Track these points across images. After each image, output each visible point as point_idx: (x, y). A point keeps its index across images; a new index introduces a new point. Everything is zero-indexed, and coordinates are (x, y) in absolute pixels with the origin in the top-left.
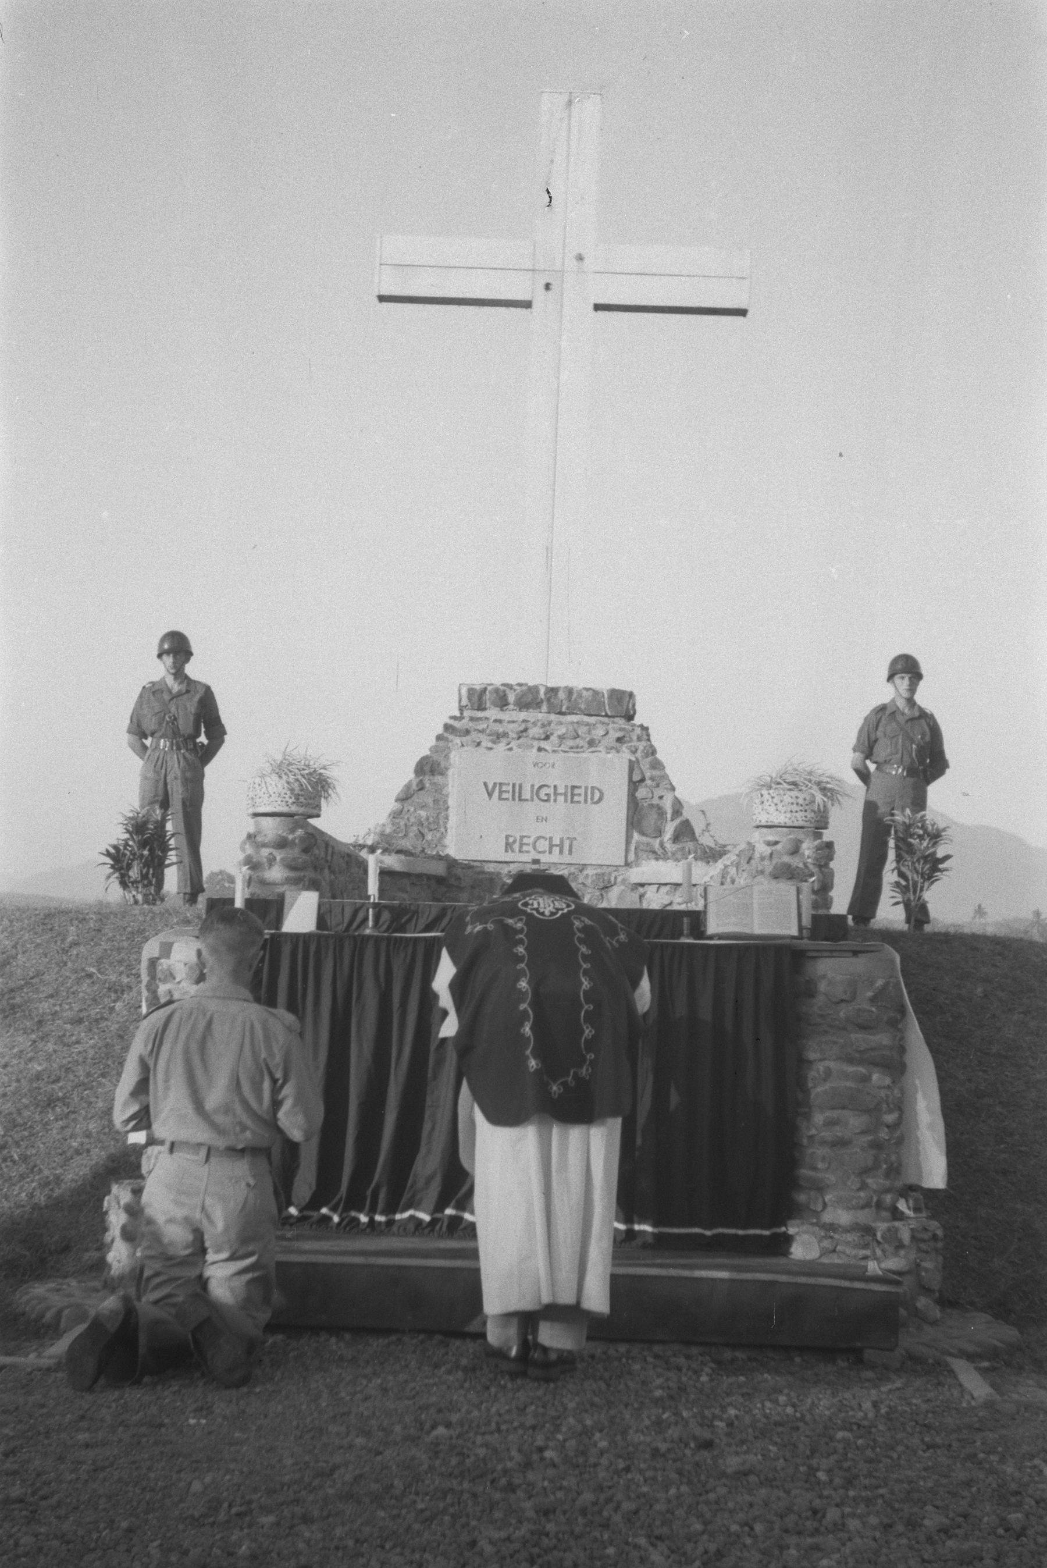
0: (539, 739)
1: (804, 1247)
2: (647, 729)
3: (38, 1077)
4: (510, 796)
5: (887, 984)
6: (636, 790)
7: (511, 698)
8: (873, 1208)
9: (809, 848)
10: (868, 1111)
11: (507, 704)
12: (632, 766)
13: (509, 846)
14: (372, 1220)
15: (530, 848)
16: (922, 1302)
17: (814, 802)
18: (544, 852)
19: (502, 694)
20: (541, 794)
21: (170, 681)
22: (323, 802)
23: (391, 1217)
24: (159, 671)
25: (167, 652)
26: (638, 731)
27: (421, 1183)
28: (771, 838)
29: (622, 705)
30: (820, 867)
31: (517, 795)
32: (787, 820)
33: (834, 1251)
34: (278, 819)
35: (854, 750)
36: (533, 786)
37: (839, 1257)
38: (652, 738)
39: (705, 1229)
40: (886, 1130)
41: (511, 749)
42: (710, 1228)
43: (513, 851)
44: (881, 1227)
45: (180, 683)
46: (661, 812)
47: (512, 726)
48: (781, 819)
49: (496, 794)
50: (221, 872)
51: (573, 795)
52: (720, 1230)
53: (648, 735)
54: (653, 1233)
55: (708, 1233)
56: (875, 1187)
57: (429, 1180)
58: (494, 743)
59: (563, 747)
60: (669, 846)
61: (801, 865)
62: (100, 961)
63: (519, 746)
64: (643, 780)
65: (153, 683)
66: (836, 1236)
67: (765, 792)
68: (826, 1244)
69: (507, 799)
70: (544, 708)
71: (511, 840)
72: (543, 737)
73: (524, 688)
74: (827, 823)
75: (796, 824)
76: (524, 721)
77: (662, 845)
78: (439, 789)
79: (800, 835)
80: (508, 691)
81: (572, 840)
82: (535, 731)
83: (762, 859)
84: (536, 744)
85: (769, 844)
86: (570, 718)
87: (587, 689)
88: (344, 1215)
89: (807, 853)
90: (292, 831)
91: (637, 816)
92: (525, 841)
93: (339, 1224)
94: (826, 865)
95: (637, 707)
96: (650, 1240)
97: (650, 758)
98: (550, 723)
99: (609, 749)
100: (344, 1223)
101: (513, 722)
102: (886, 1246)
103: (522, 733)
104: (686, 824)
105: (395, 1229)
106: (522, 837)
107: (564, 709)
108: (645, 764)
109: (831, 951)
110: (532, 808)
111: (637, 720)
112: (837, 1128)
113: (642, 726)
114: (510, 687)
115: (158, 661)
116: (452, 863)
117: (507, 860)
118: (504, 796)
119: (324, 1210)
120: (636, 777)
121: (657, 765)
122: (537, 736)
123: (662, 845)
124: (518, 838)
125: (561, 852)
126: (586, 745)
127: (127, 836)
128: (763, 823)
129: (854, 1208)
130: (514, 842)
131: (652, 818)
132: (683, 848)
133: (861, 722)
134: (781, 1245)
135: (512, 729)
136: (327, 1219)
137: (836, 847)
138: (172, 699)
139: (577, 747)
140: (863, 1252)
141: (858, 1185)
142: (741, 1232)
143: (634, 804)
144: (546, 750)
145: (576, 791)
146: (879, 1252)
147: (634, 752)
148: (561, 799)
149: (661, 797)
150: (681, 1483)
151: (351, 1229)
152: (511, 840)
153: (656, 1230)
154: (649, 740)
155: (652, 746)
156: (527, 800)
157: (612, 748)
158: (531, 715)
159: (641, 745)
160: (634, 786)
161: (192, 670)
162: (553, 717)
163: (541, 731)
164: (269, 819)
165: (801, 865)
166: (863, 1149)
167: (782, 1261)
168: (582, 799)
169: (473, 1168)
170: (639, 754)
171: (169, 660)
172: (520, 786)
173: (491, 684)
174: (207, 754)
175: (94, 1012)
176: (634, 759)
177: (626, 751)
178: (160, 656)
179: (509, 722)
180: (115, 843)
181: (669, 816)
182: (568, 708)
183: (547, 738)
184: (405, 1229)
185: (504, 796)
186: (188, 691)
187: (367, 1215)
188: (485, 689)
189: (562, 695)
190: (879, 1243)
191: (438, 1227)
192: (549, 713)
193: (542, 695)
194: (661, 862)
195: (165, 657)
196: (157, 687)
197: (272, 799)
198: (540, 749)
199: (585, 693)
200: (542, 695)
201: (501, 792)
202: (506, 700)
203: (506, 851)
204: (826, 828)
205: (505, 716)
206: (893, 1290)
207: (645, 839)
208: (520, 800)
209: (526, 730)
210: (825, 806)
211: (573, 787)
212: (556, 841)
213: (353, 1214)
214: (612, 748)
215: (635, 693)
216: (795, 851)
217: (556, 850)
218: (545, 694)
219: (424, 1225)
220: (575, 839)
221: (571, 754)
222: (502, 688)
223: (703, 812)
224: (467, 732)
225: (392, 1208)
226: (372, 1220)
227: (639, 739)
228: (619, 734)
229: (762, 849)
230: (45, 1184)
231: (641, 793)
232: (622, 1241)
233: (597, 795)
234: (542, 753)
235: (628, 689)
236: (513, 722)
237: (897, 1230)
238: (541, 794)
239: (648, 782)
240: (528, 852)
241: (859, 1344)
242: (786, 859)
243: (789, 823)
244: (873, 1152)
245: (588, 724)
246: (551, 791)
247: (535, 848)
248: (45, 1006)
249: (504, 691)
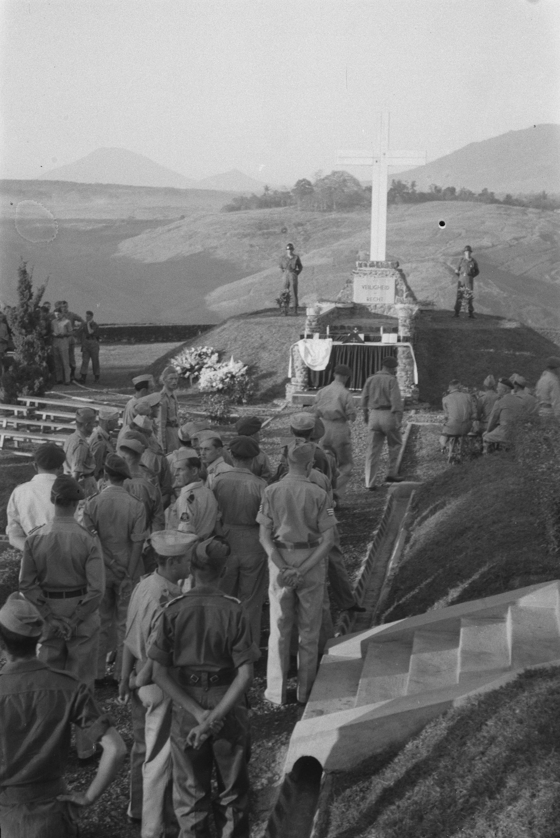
3: (271, 362)
12: (396, 281)
13: (368, 300)
16: (414, 401)
44: (407, 390)
50: (304, 180)
60: (405, 299)
62: (279, 337)
78: (352, 287)
82: (374, 273)
103: (371, 273)
116: (355, 304)
131: (400, 293)
150: (525, 479)
160: (396, 285)
174: (298, 273)
175: (280, 349)
224: (358, 273)
230: (274, 382)
231: (398, 287)
248: (270, 347)
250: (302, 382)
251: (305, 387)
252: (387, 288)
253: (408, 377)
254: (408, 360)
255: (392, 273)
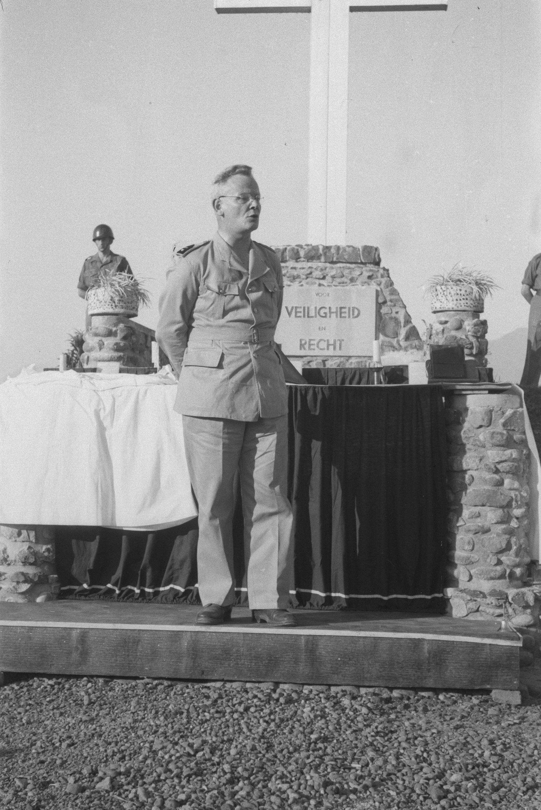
0: (319, 279)
1: (459, 607)
2: (388, 270)
4: (302, 314)
5: (515, 413)
6: (381, 308)
7: (302, 253)
8: (508, 580)
9: (469, 325)
10: (502, 507)
11: (299, 258)
13: (302, 346)
14: (143, 592)
15: (315, 347)
17: (472, 293)
18: (324, 349)
19: (296, 251)
20: (322, 313)
21: (101, 255)
22: (141, 305)
23: (157, 589)
24: (94, 249)
25: (99, 239)
26: (381, 271)
27: (176, 566)
28: (443, 319)
29: (371, 257)
30: (477, 338)
31: (306, 314)
32: (454, 306)
33: (477, 611)
34: (106, 317)
35: (523, 283)
36: (316, 308)
37: (482, 615)
38: (390, 276)
39: (383, 595)
40: (515, 520)
41: (302, 285)
42: (387, 595)
43: (305, 349)
45: (107, 257)
46: (396, 320)
47: (302, 271)
48: (451, 305)
49: (293, 313)
51: (341, 313)
52: (394, 596)
53: (388, 274)
54: (346, 599)
55: (385, 598)
56: (508, 562)
57: (182, 562)
58: (291, 282)
59: (334, 283)
60: (403, 343)
61: (464, 337)
63: (307, 283)
64: (385, 302)
65: (92, 257)
66: (479, 600)
67: (438, 288)
68: (472, 605)
69: (300, 317)
70: (323, 259)
71: (303, 342)
72: (322, 277)
73: (310, 247)
74: (483, 308)
75: (460, 308)
76: (310, 268)
77: (398, 342)
79: (463, 316)
80: (300, 249)
81: (341, 341)
82: (317, 274)
83: (437, 334)
84: (317, 282)
85: (441, 323)
86: (339, 265)
87: (349, 247)
88: (123, 588)
89: (468, 328)
90: (116, 325)
91: (381, 325)
92: (312, 342)
93: (119, 595)
94: (483, 336)
95: (381, 256)
96: (345, 605)
97: (390, 288)
98: (326, 268)
99: (363, 284)
100: (124, 593)
101: (303, 268)
102: (516, 606)
104: (414, 329)
105: (159, 598)
106: (310, 340)
107: (335, 259)
108: (386, 292)
109: (473, 390)
110: (317, 322)
111: (382, 265)
112: (479, 520)
113: (384, 269)
114: (301, 247)
115: (93, 242)
117: (302, 354)
118: (299, 315)
119: (109, 586)
120: (381, 300)
121: (394, 292)
122: (318, 277)
123: (398, 342)
124: (308, 341)
125: (335, 349)
126: (349, 281)
127: (73, 348)
128: (438, 309)
129: (492, 578)
130: (305, 343)
131: (391, 326)
132: (411, 345)
133: (527, 265)
134: (441, 608)
135: (302, 273)
136: (112, 591)
137: (488, 323)
138: (102, 266)
139: (343, 283)
140: (499, 611)
141: (496, 562)
142: (410, 597)
143: (379, 316)
144: (323, 285)
145: (343, 310)
146: (510, 610)
147: (379, 285)
148: (333, 315)
149: (397, 313)
151: (128, 599)
152: (303, 342)
153: (347, 597)
154: (389, 277)
155: (390, 280)
156: (312, 317)
157: (365, 282)
158: (314, 264)
159: (384, 280)
160: (379, 306)
161: (114, 248)
162: (328, 265)
163: (320, 273)
164: (100, 318)
165: (464, 337)
166: (498, 535)
167: (442, 619)
168: (347, 315)
169: (255, 549)
170: (382, 286)
171: (100, 243)
172: (308, 308)
173: (289, 246)
176: (379, 289)
177: (374, 284)
178: (94, 240)
179: (300, 268)
180: (67, 352)
181: (402, 324)
182: (337, 259)
183: (324, 278)
184: (166, 599)
185: (299, 315)
186: (111, 261)
187: (139, 589)
188: (286, 249)
189: (333, 251)
190: (510, 604)
191: (189, 597)
192: (325, 262)
193: (321, 251)
194: (396, 352)
195: (97, 241)
196: (94, 259)
197: (102, 303)
198: (320, 285)
199: (347, 249)
200: (321, 251)
201: (296, 312)
202: (299, 255)
203: (301, 349)
204: (482, 312)
205: (299, 265)
206: (515, 645)
207: (387, 339)
208: (308, 317)
209: (311, 273)
210: (479, 295)
211: (341, 308)
212: (332, 342)
213: (129, 587)
214: (365, 282)
215: (380, 248)
216: (459, 328)
217: (331, 348)
218: (323, 250)
219: (180, 595)
220: (343, 340)
221: (339, 287)
222: (296, 248)
223: (424, 321)
225: (156, 583)
226: (143, 592)
227: (382, 276)
228: (370, 274)
229: (438, 327)
232: (323, 605)
233: (356, 312)
234: (322, 287)
235: (375, 246)
236: (303, 268)
237: (524, 594)
238: (322, 313)
239: (389, 303)
240: (314, 349)
241: (488, 687)
242: (454, 333)
243: (456, 308)
244: (507, 536)
245: (349, 268)
246: (327, 311)
247: (318, 347)
249: (298, 250)
250: (25, 562)
251: (36, 585)
252: (355, 313)
253: (511, 532)
254: (513, 453)
255: (366, 274)
